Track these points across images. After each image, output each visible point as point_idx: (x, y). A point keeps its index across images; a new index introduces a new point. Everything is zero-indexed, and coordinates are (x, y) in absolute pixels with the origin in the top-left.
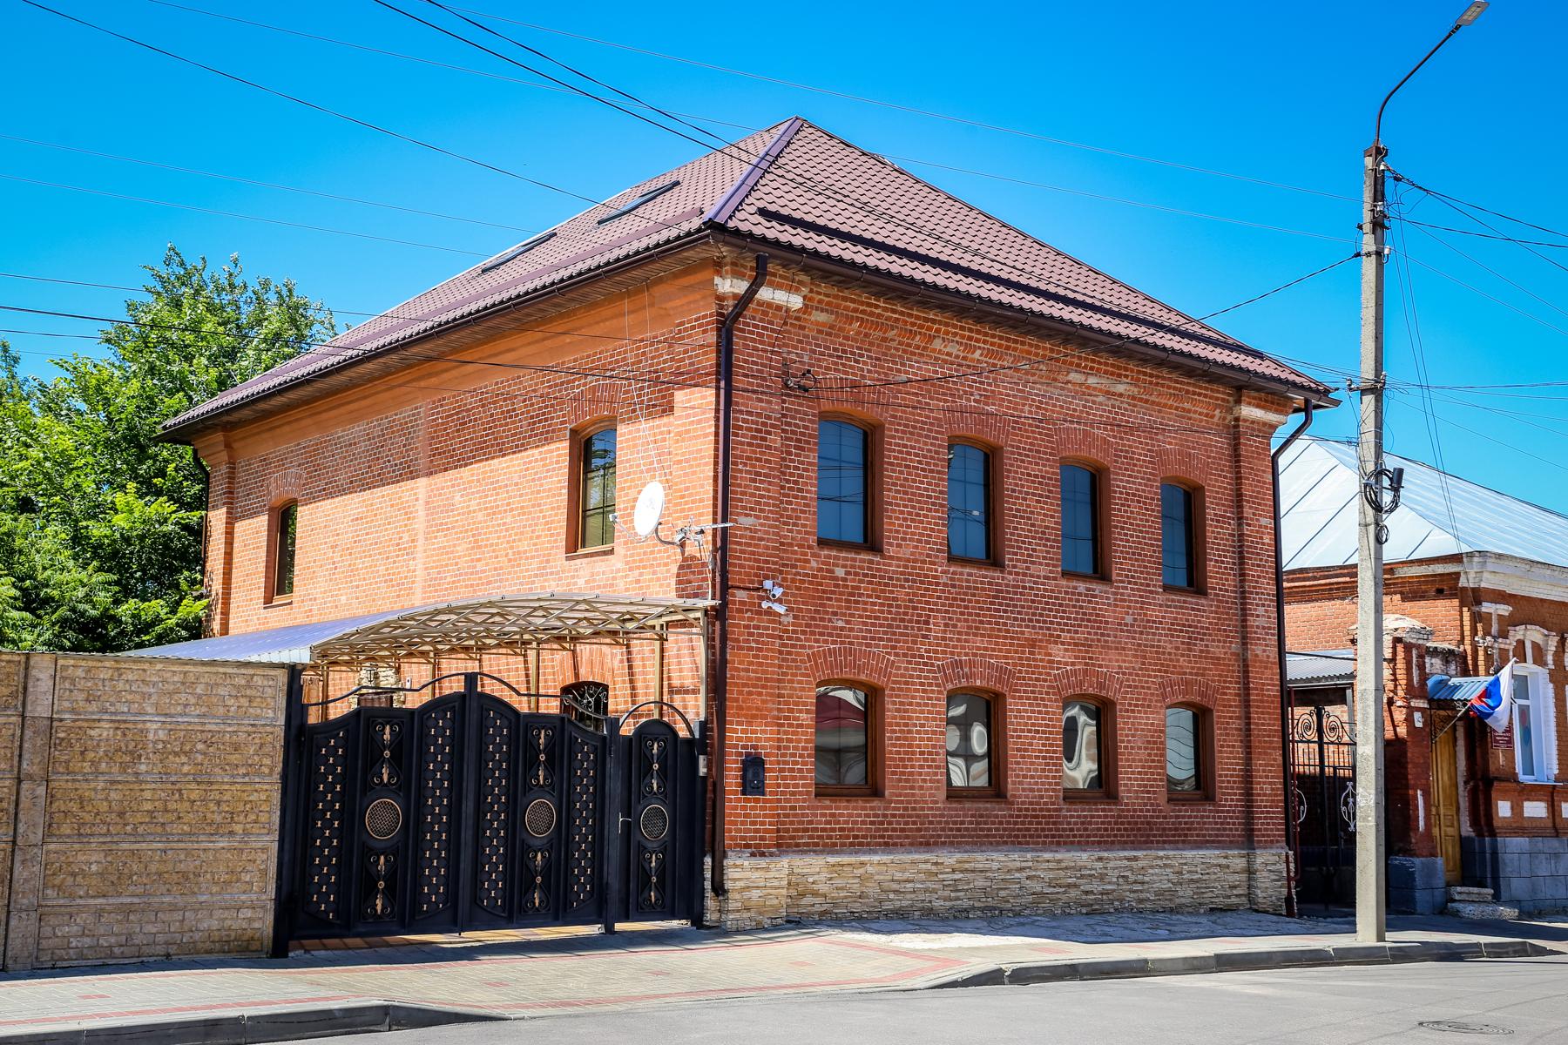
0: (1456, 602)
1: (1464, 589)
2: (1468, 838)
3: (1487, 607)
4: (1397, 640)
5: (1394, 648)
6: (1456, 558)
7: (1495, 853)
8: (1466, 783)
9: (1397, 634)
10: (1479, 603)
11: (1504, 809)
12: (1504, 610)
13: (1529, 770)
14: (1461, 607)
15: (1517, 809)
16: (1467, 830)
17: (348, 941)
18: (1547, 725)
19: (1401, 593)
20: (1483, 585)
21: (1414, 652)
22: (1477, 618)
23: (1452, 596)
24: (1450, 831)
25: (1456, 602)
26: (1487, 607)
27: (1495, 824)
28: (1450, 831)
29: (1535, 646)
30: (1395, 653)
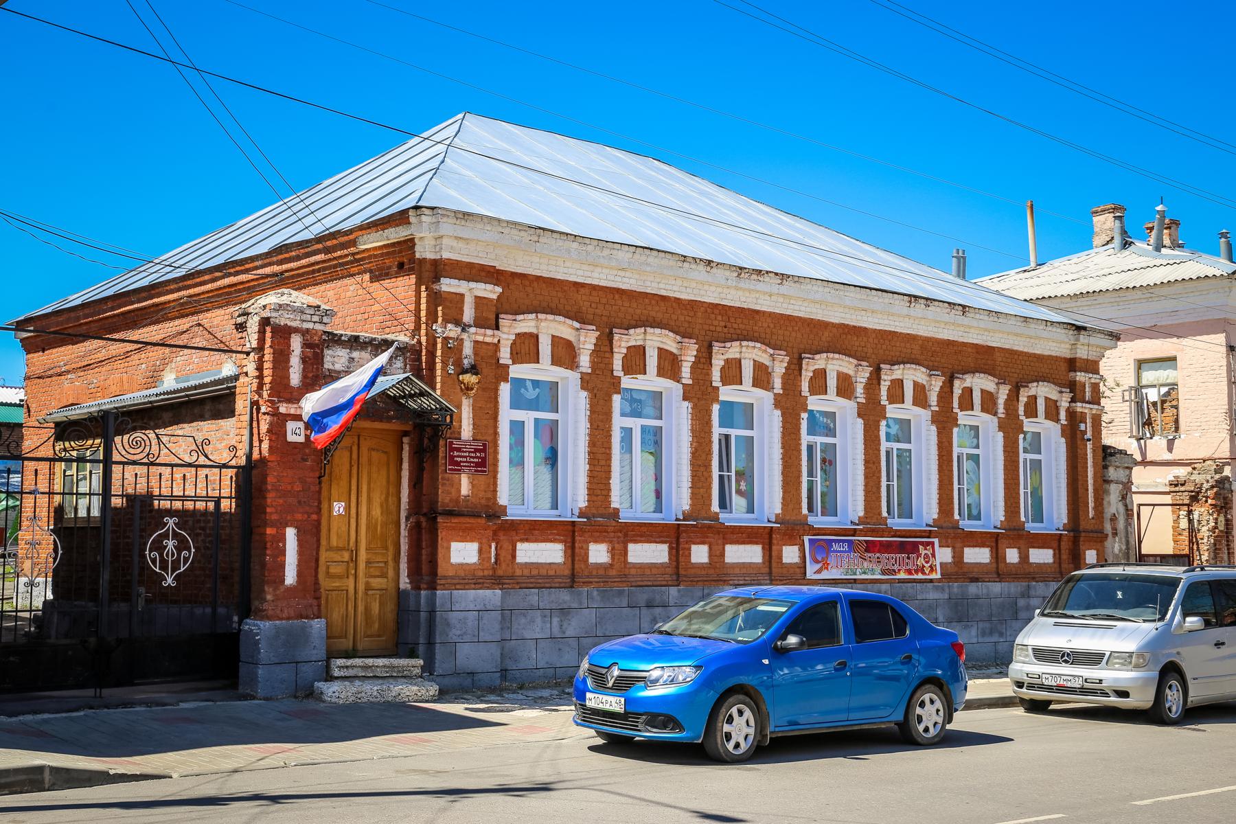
0: (413, 279)
1: (423, 261)
2: (405, 591)
3: (448, 285)
4: (265, 322)
5: (262, 333)
6: (401, 218)
7: (432, 612)
8: (407, 518)
9: (266, 314)
10: (437, 279)
11: (463, 552)
12: (491, 291)
13: (1038, 517)
14: (418, 285)
15: (619, 553)
16: (405, 583)
17: (106, 692)
18: (576, 446)
19: (371, 271)
20: (1078, 355)
21: (296, 343)
22: (436, 299)
23: (411, 271)
24: (377, 582)
25: (413, 279)
26: (448, 285)
27: (440, 571)
28: (377, 582)
29: (916, 385)
30: (261, 340)
